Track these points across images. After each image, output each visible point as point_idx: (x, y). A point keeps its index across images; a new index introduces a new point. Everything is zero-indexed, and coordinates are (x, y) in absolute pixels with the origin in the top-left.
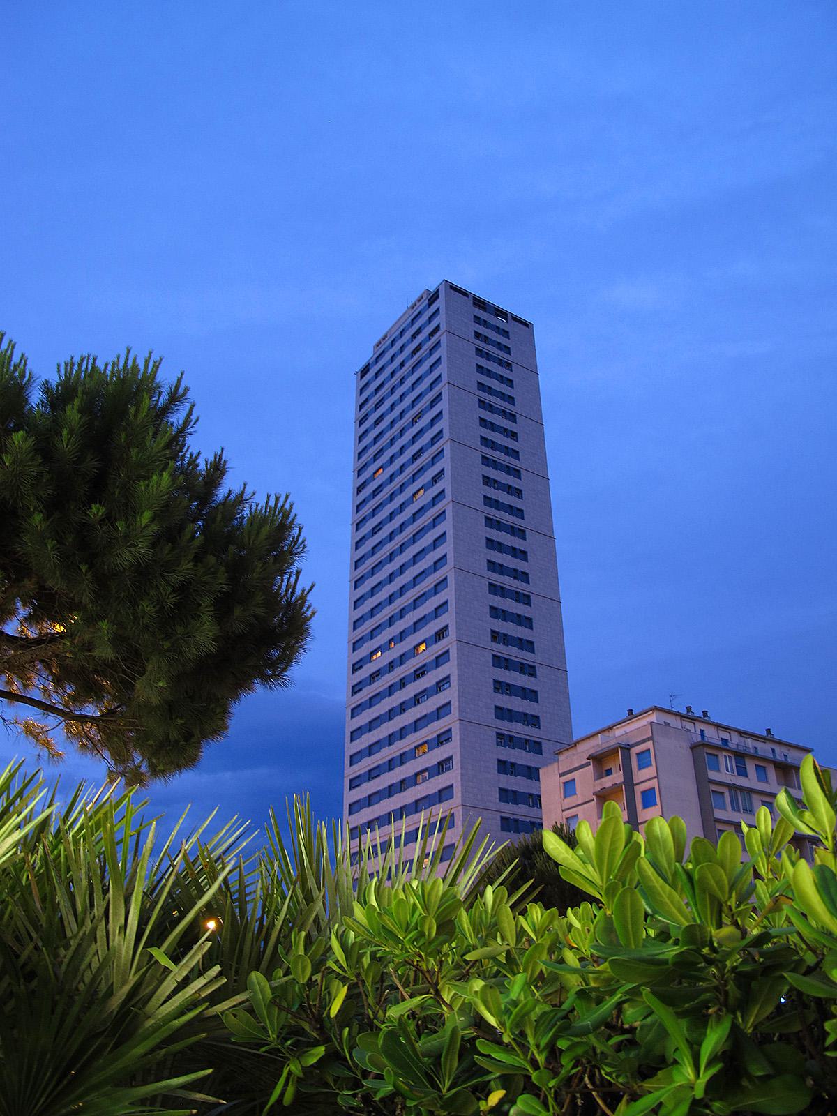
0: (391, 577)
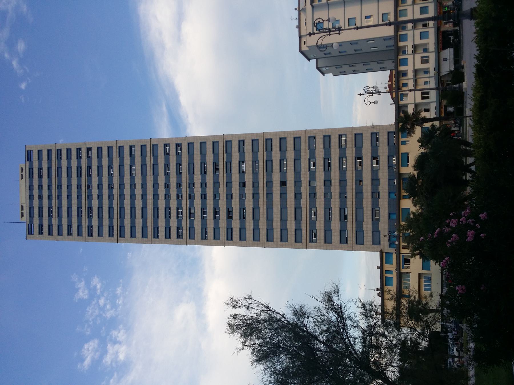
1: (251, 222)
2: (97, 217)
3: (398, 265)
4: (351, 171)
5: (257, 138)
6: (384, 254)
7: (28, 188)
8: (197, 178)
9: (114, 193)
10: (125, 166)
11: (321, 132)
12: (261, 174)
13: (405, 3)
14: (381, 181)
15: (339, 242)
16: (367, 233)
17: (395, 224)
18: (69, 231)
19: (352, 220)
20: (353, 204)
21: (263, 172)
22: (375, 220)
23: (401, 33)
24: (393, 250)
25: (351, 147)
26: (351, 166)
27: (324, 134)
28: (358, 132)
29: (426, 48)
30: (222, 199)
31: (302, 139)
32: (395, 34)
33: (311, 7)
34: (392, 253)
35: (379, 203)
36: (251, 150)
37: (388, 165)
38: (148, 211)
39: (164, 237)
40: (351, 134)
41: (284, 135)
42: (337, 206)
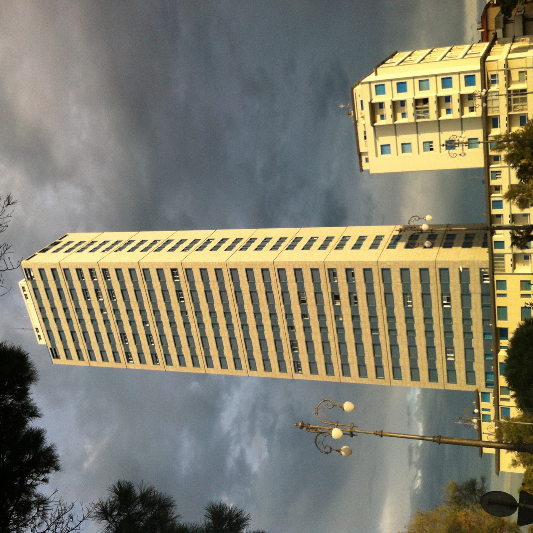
0: (93, 321)
1: (321, 356)
2: (134, 343)
3: (483, 81)
4: (437, 309)
5: (317, 268)
6: (480, 394)
7: (38, 310)
8: (247, 307)
9: (146, 308)
10: (156, 291)
13: (496, 78)
14: (474, 320)
15: (428, 380)
16: (460, 373)
17: (492, 367)
18: (86, 296)
19: (441, 359)
20: (442, 342)
21: (329, 305)
22: (468, 334)
23: (497, 278)
24: (491, 390)
25: (435, 282)
26: (437, 303)
27: (401, 267)
28: (444, 267)
29: (524, 116)
30: (277, 294)
31: (374, 271)
32: (481, 68)
33: (372, 128)
34: (489, 393)
35: (473, 343)
36: (311, 280)
37: (482, 304)
38: (195, 340)
39: (220, 367)
40: (441, 353)
41: (350, 265)
42: (423, 344)
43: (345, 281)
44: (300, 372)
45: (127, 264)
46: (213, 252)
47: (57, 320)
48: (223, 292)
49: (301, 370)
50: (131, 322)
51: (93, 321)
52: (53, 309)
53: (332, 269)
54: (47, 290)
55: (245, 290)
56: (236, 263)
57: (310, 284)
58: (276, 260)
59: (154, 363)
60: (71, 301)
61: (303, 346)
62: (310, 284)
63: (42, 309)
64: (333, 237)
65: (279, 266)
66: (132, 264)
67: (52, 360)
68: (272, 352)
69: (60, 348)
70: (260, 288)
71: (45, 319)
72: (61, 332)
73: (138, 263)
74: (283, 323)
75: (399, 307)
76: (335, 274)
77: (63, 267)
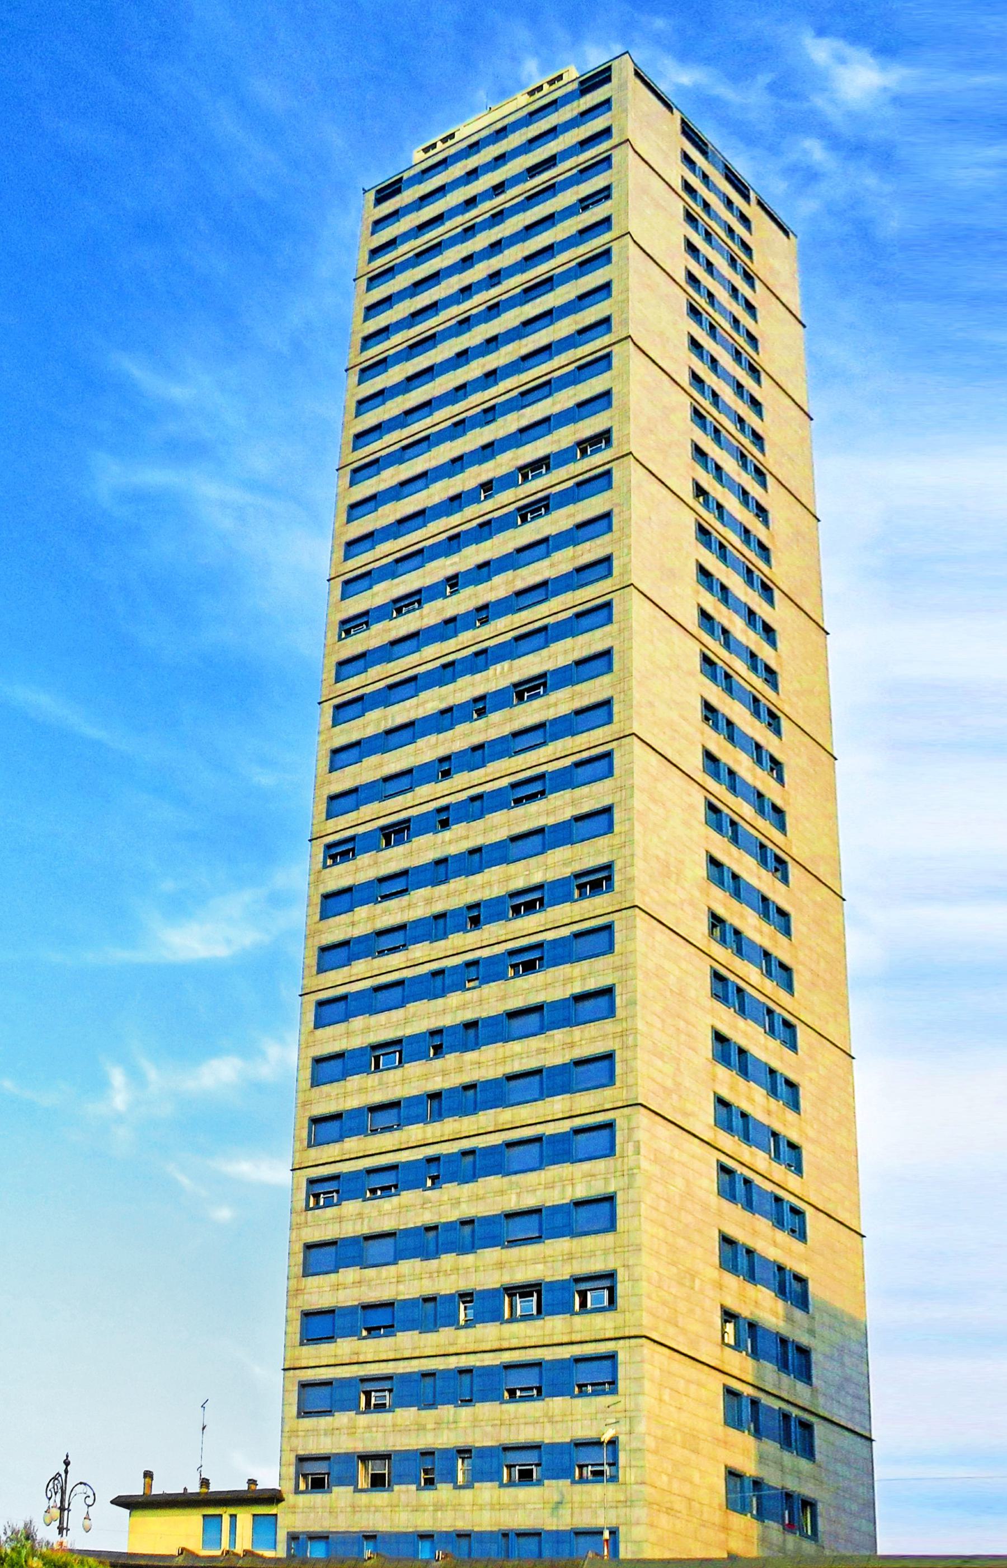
11: (626, 1177)
12: (504, 931)
19: (362, 1359)
43: (578, 989)
44: (343, 635)
45: (626, 691)
46: (686, 341)
47: (458, 463)
48: (543, 590)
49: (335, 863)
50: (456, 498)
51: (458, 463)
52: (484, 613)
53: (609, 879)
54: (545, 425)
55: (550, 657)
56: (627, 669)
57: (565, 864)
58: (638, 953)
59: (343, 622)
60: (522, 194)
61: (405, 628)
62: (565, 864)
63: (502, 133)
64: (724, 1385)
65: (619, 810)
66: (625, 322)
67: (372, 188)
68: (381, 765)
69: (402, 200)
70: (556, 705)
71: (475, 147)
72: (421, 516)
73: (627, 454)
74: (459, 788)
75: (502, 1192)
76: (596, 887)
77: (615, 247)
